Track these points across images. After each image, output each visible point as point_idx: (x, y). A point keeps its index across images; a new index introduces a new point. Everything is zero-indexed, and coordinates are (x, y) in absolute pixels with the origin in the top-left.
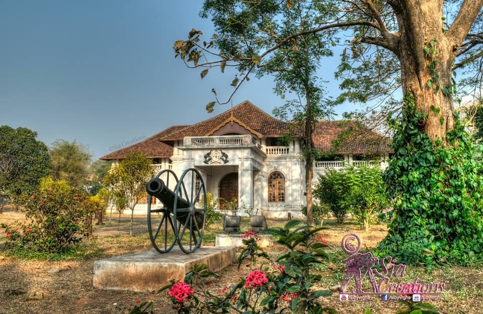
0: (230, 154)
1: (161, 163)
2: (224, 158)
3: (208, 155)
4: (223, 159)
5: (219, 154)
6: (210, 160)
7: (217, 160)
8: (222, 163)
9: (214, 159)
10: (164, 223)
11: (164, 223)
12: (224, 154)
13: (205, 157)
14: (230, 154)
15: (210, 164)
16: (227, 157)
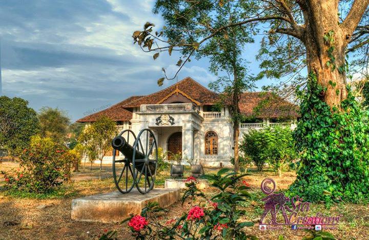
0: (176, 117)
1: (123, 125)
2: (171, 121)
3: (159, 118)
4: (170, 122)
5: (167, 118)
6: (160, 122)
7: (165, 122)
8: (170, 125)
9: (164, 122)
10: (125, 171)
11: (125, 171)
12: (171, 118)
13: (157, 120)
14: (176, 117)
15: (160, 125)
16: (173, 120)
